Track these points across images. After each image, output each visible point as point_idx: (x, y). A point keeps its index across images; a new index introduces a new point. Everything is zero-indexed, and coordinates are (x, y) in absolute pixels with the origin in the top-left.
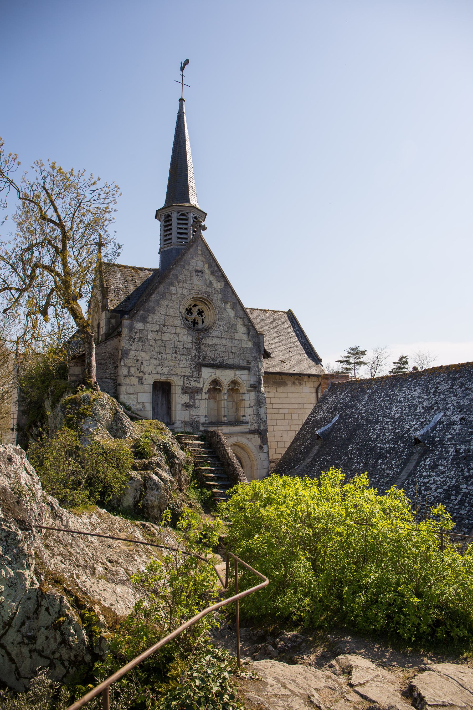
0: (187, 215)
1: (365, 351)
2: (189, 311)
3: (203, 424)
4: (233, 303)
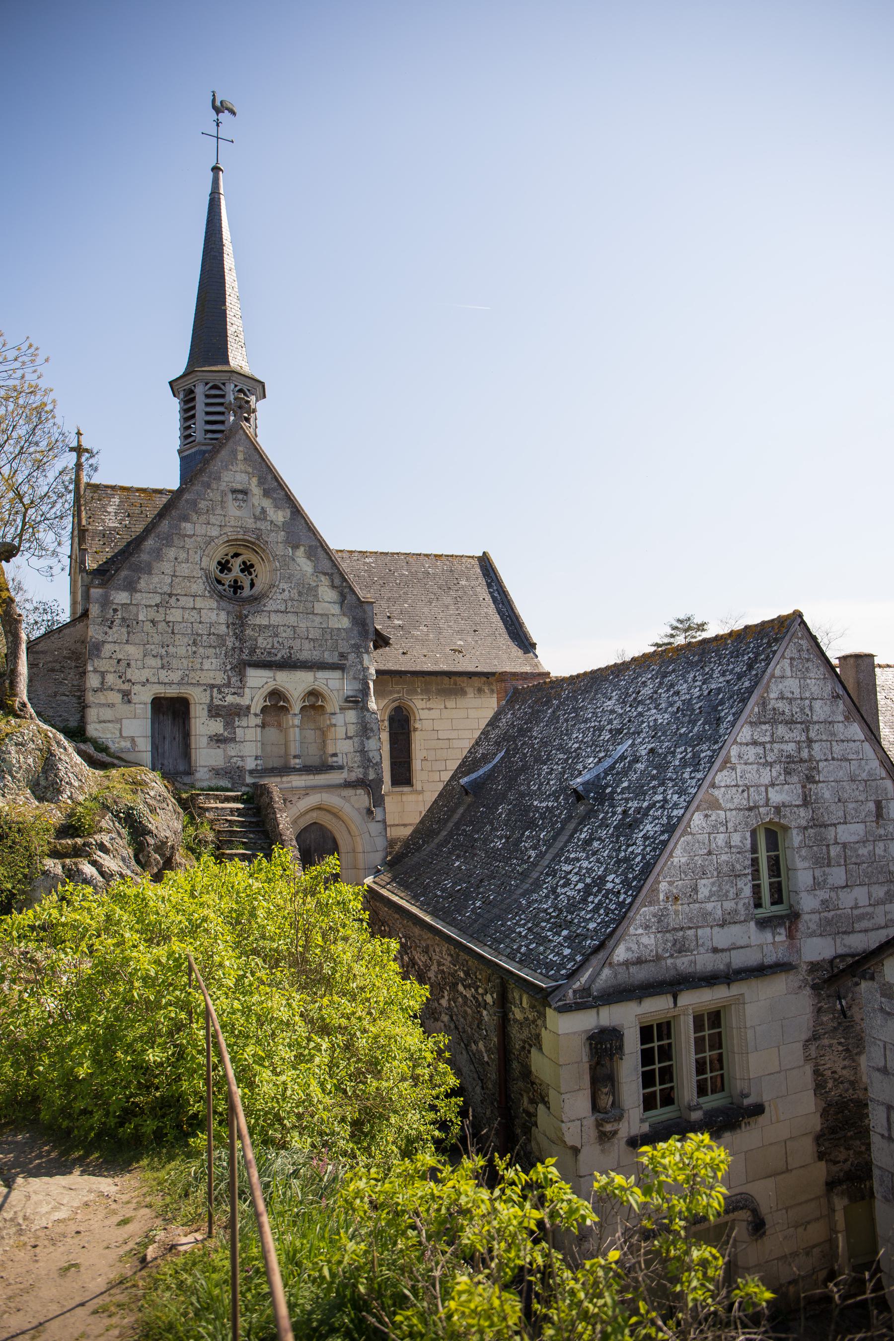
0: (223, 387)
1: (703, 624)
2: (224, 566)
3: (251, 772)
4: (310, 547)
